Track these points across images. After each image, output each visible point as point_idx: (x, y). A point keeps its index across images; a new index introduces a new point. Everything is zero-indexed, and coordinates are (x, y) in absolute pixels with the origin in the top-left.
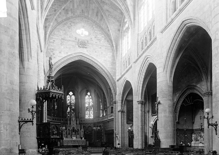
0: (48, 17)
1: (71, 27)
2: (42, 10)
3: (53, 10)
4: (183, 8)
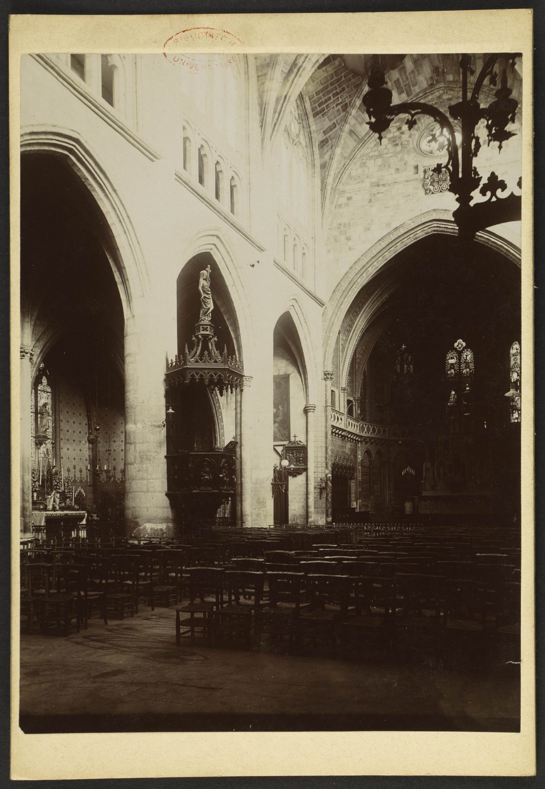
0: (327, 136)
1: (400, 137)
2: (264, 131)
3: (339, 107)
4: (125, 132)
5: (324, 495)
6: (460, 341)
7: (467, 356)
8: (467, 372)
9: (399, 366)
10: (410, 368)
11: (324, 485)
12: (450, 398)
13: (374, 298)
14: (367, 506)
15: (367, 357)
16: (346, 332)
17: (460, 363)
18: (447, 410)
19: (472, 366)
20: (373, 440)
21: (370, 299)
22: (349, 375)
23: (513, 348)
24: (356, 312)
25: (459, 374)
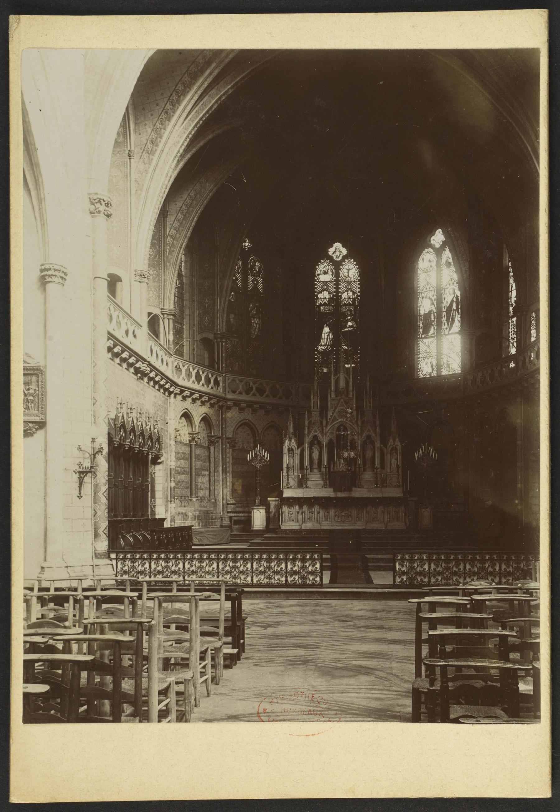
5: (88, 488)
6: (338, 245)
7: (348, 270)
8: (349, 298)
9: (239, 276)
10: (258, 282)
11: (87, 464)
12: (321, 338)
13: (203, 83)
14: (185, 516)
15: (186, 235)
16: (145, 155)
17: (337, 282)
18: (316, 358)
19: (356, 287)
20: (196, 396)
21: (194, 84)
22: (153, 245)
23: (423, 259)
24: (166, 113)
25: (336, 300)
